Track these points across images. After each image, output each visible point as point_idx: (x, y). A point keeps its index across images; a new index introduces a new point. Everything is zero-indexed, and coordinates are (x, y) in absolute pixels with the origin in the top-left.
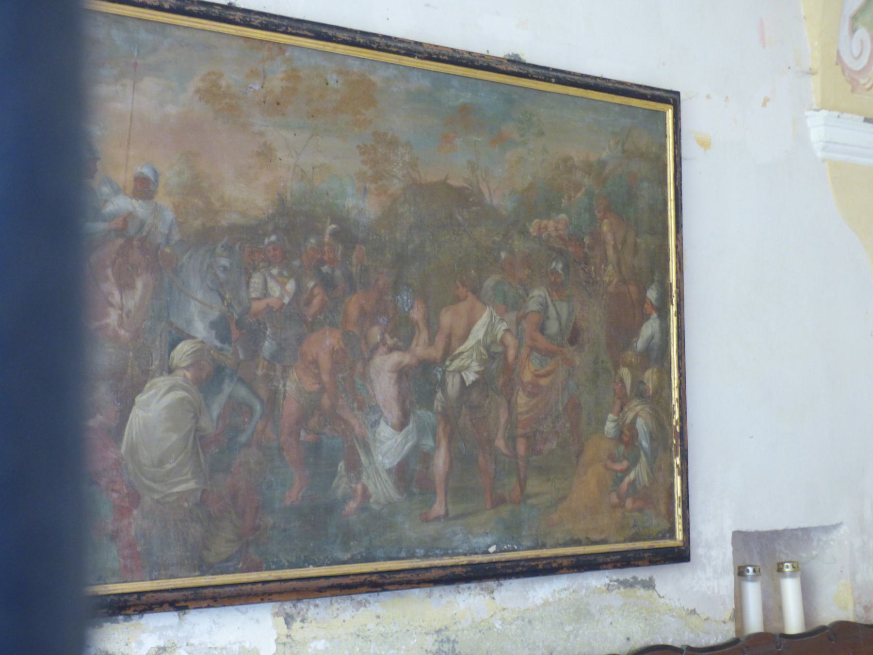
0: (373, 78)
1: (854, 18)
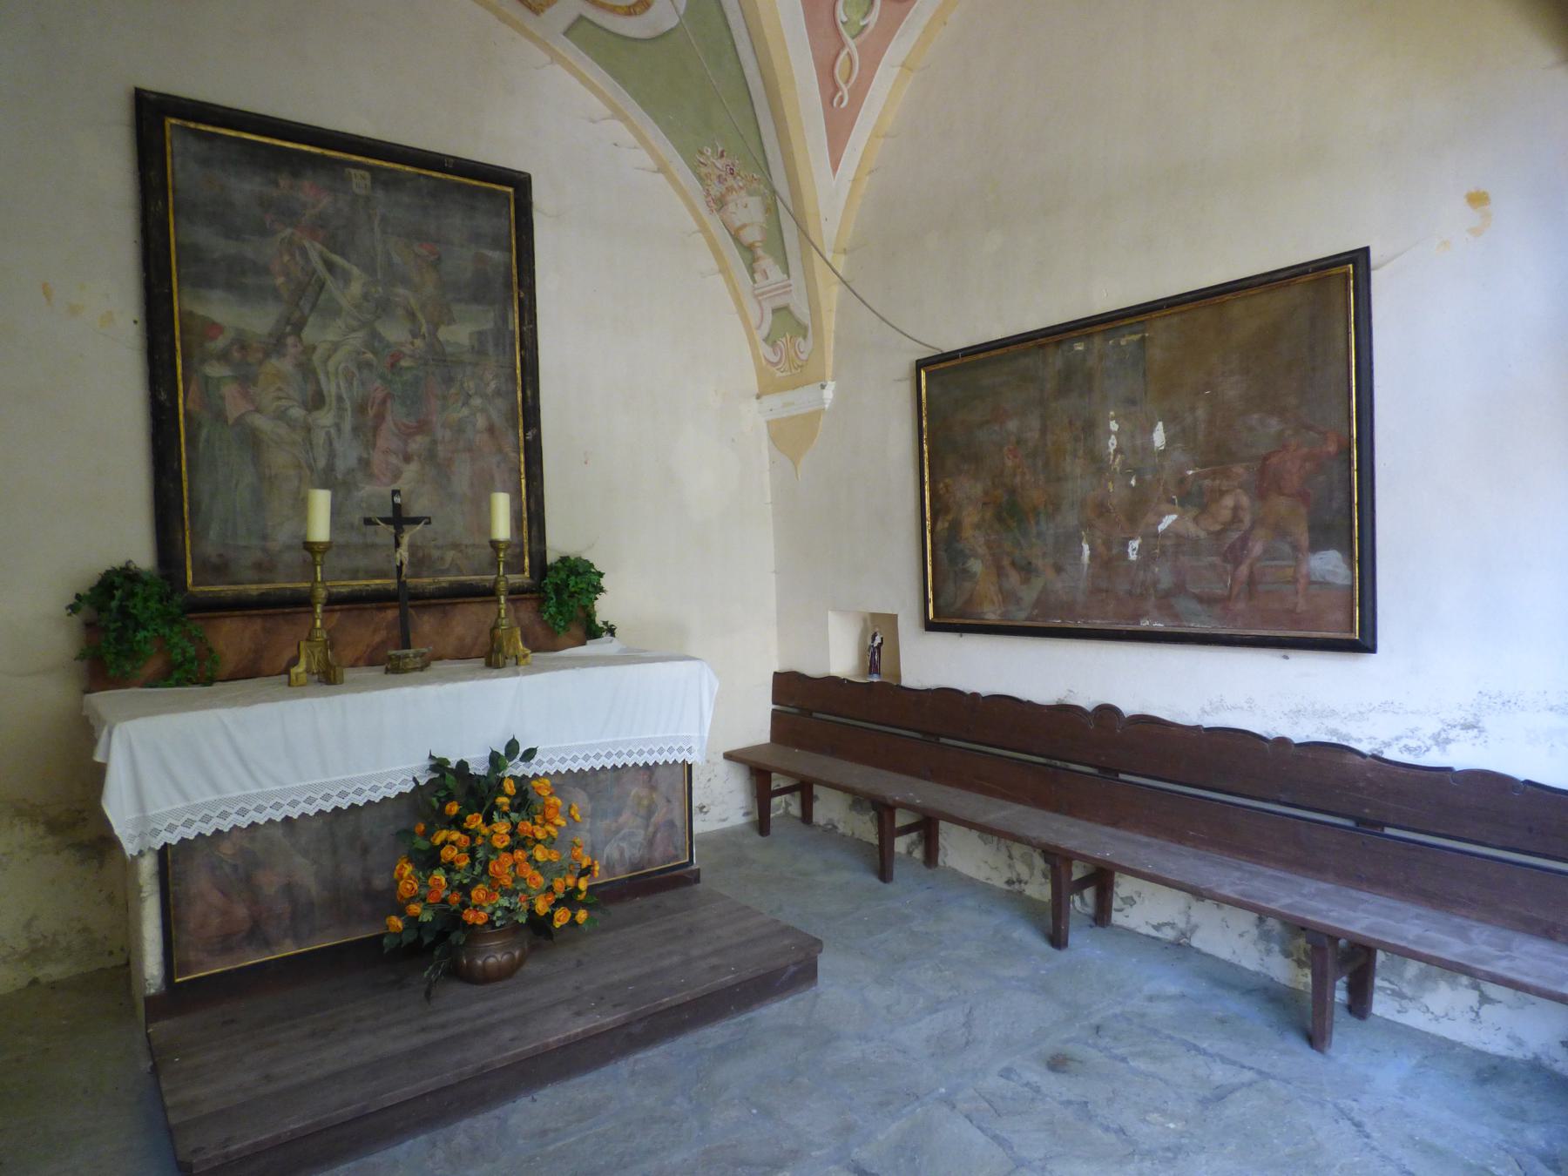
0: (300, 440)
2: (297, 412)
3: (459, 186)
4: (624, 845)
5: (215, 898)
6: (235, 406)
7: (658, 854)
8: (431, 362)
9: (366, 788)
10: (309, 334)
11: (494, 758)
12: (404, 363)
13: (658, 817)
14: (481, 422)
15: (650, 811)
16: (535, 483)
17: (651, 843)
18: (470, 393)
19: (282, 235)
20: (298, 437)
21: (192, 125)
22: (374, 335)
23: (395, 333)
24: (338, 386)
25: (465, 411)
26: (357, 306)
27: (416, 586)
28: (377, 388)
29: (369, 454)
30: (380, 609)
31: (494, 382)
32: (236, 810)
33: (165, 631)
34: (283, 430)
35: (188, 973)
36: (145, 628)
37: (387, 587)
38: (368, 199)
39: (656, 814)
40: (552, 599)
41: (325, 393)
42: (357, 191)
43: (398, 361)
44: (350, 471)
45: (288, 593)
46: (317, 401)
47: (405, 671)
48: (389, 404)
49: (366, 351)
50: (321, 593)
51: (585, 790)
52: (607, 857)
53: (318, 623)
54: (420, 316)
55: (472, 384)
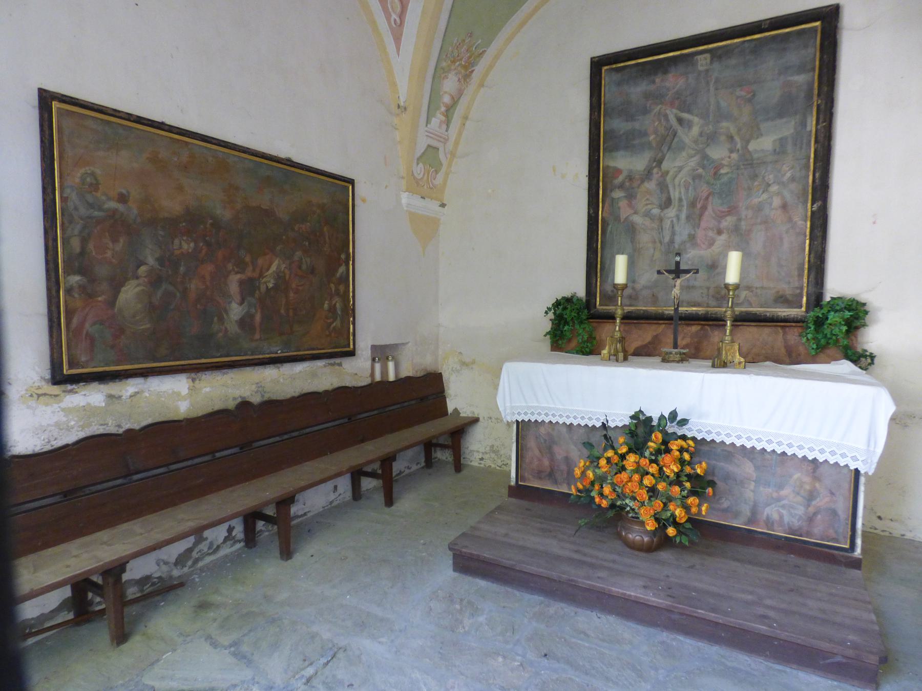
0: (656, 226)
1: (418, 159)
2: (656, 211)
3: (774, 37)
4: (784, 512)
5: (537, 452)
6: (624, 211)
7: (817, 530)
8: (742, 167)
9: (806, 447)
10: (665, 165)
11: (662, 417)
12: (723, 171)
13: (822, 501)
14: (777, 202)
15: (811, 496)
16: (816, 243)
17: (811, 520)
18: (770, 183)
19: (655, 111)
20: (655, 225)
21: (614, 66)
22: (705, 157)
23: (718, 153)
24: (680, 193)
25: (765, 196)
26: (696, 142)
27: (717, 312)
28: (704, 190)
29: (695, 231)
30: (688, 325)
31: (790, 172)
32: (706, 430)
33: (577, 327)
34: (648, 222)
35: (525, 482)
36: (568, 325)
37: (698, 312)
38: (707, 71)
39: (818, 499)
40: (810, 328)
41: (672, 197)
42: (700, 68)
43: (719, 170)
44: (683, 243)
45: (642, 312)
46: (668, 203)
47: (668, 362)
48: (711, 198)
49: (698, 168)
50: (619, 312)
51: (752, 461)
52: (768, 515)
53: (617, 328)
54: (737, 139)
55: (771, 176)
